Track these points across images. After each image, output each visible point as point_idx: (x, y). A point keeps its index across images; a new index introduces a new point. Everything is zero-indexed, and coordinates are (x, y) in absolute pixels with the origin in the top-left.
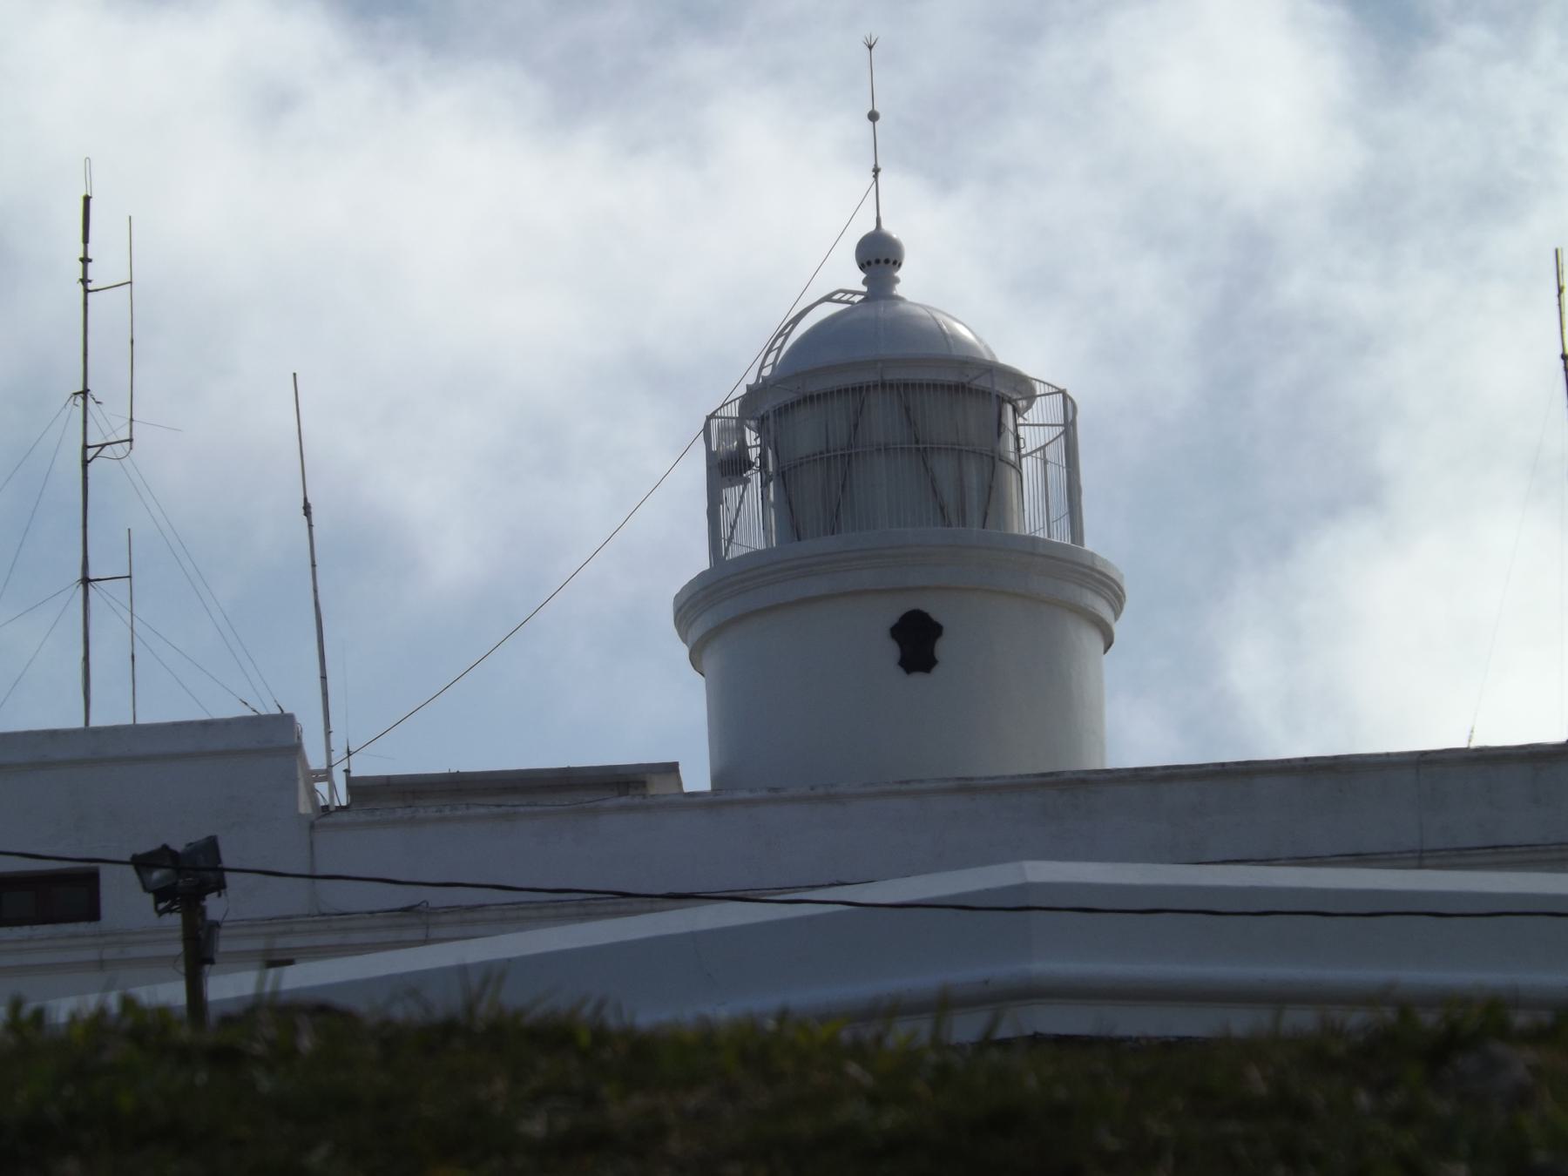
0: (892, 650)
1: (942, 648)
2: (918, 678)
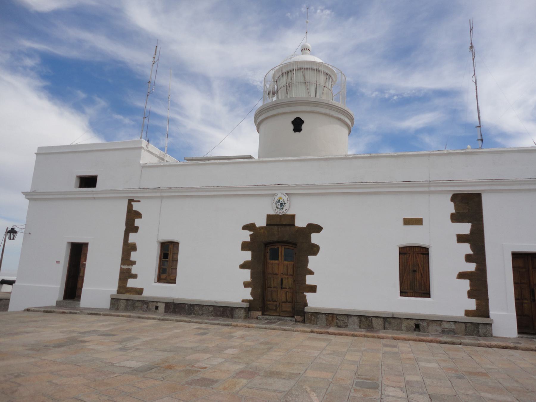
0: (292, 127)
1: (303, 127)
2: (297, 133)
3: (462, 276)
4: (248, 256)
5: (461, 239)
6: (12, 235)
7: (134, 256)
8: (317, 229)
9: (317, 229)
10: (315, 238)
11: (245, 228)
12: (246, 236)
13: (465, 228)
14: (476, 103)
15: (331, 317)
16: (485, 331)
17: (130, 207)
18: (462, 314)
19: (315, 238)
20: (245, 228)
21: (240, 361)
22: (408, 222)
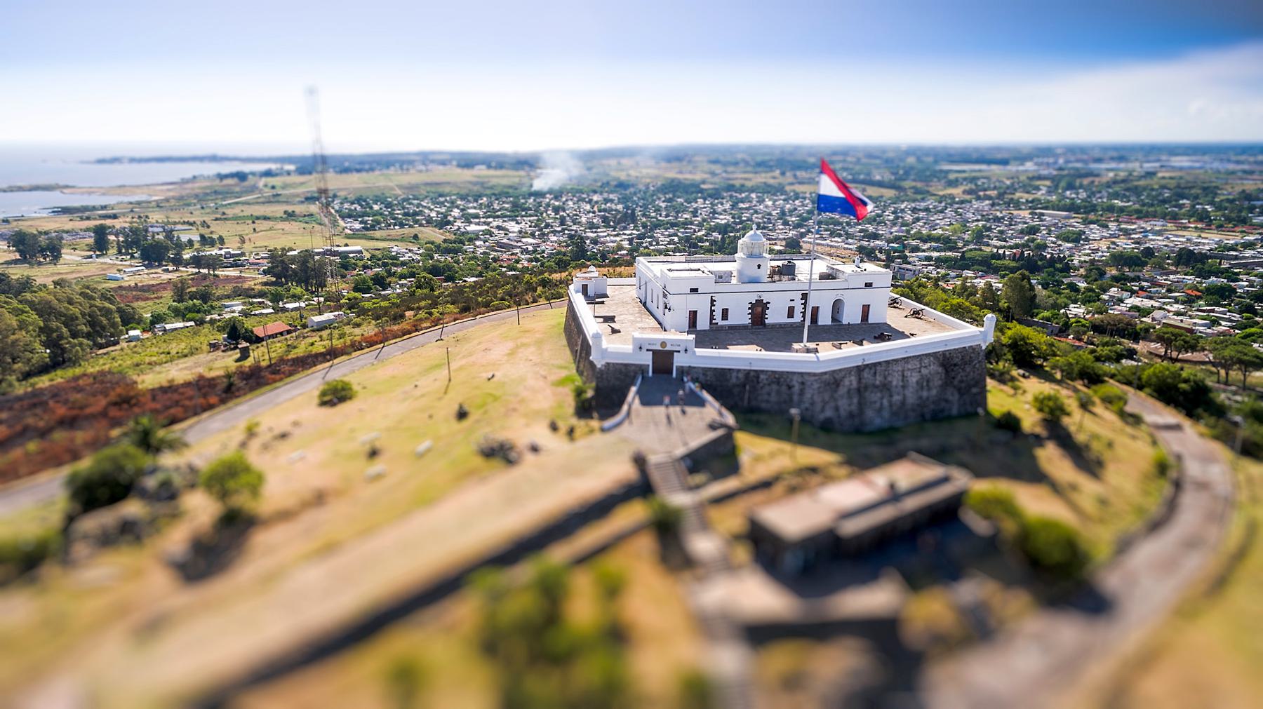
3: (801, 312)
4: (766, 316)
5: (802, 304)
6: (1143, 374)
7: (714, 313)
8: (769, 303)
9: (769, 303)
10: (768, 305)
11: (750, 303)
12: (750, 306)
13: (803, 301)
14: (154, 165)
15: (527, 425)
16: (1040, 287)
17: (712, 298)
18: (190, 438)
19: (768, 305)
20: (750, 303)
21: (1216, 338)
22: (791, 300)
